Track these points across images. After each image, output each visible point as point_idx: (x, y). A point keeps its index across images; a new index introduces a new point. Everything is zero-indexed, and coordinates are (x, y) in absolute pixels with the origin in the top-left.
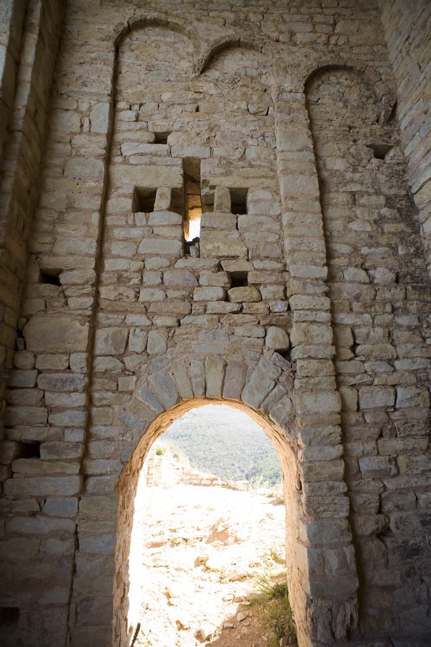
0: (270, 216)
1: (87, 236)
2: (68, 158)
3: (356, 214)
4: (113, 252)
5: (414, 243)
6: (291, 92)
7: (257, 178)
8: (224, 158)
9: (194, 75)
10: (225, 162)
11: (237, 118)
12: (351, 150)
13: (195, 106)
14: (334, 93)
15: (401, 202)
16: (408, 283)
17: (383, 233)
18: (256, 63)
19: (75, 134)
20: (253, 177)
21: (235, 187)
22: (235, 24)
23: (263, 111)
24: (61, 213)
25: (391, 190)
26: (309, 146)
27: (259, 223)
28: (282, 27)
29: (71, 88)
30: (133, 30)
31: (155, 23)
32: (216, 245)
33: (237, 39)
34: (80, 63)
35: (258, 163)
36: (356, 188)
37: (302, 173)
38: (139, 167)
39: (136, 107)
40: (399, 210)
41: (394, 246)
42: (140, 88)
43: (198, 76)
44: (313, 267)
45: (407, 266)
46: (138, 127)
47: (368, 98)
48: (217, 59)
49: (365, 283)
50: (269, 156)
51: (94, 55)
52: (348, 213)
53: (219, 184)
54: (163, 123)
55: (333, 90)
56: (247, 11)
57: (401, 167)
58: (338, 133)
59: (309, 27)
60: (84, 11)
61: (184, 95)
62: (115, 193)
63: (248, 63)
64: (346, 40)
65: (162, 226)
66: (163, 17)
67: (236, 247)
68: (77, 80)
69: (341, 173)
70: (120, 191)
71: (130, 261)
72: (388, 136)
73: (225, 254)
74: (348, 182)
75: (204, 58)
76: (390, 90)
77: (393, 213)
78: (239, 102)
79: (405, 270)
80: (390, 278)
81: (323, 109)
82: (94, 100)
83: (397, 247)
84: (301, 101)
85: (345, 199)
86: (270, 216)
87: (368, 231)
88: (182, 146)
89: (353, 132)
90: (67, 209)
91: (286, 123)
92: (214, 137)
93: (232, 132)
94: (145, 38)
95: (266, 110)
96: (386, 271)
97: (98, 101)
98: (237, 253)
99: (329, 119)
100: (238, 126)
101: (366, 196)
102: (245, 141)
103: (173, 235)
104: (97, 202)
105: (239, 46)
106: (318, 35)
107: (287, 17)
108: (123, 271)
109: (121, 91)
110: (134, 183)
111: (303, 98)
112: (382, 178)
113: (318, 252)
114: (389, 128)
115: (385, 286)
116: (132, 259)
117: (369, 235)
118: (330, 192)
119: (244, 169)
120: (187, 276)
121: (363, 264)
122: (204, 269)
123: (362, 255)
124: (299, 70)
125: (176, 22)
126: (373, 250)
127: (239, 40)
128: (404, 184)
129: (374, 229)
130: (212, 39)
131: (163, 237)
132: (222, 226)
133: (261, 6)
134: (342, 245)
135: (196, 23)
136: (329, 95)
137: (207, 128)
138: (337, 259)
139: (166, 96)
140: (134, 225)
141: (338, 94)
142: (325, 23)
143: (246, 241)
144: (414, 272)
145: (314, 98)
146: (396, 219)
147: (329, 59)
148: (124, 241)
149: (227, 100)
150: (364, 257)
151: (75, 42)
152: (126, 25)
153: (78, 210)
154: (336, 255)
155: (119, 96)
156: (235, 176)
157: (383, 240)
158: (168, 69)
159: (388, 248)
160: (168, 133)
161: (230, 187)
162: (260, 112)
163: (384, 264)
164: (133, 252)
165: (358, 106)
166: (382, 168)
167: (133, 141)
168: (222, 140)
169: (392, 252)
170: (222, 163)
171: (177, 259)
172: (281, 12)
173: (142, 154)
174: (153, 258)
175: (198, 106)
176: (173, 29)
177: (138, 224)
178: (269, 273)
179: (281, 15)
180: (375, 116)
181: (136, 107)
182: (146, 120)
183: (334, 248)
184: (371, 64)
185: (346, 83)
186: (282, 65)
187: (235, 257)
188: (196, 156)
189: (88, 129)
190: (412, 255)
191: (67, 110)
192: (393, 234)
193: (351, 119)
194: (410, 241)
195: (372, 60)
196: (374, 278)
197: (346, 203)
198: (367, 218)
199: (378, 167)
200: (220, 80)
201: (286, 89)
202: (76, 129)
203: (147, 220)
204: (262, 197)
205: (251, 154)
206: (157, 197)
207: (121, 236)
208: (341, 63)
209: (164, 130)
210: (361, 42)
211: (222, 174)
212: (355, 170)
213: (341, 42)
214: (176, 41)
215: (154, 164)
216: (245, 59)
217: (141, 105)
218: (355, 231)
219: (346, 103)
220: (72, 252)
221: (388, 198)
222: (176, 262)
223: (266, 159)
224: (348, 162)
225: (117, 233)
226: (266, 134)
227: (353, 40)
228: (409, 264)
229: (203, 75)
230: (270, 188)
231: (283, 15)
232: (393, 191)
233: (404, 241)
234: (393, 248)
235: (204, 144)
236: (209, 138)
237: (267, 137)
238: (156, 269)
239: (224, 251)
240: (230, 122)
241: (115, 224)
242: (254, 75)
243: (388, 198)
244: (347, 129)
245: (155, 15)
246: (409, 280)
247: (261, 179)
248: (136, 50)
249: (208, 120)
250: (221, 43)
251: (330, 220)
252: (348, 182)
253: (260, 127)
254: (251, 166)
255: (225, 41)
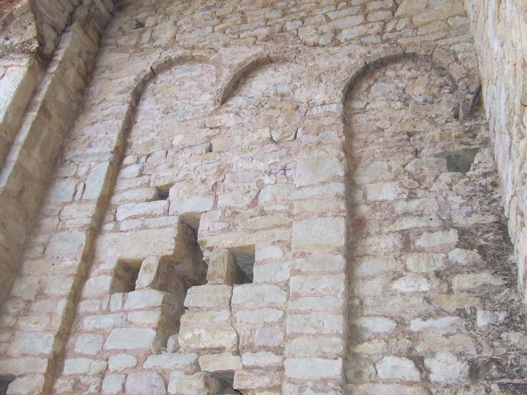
0: (277, 284)
1: (47, 330)
2: (54, 233)
3: (406, 266)
4: (76, 350)
5: (504, 305)
6: (324, 104)
7: (268, 229)
8: (230, 208)
9: (213, 108)
10: (230, 212)
11: (254, 152)
12: (408, 168)
13: (207, 145)
14: (391, 91)
15: (486, 236)
16: (492, 379)
17: (450, 292)
18: (290, 76)
19: (66, 204)
20: (262, 229)
21: (236, 246)
22: (267, 39)
23: (289, 136)
24: (29, 302)
25: (469, 218)
26: (338, 173)
27: (258, 295)
28: (325, 28)
29: (78, 152)
30: (158, 73)
31: (181, 60)
32: (197, 332)
33: (266, 56)
34: (93, 123)
35: (273, 207)
36: (407, 224)
37: (323, 215)
38: (128, 234)
39: (143, 159)
40: (482, 250)
41: (469, 312)
42: (152, 135)
43: (218, 108)
44: (320, 360)
45: (492, 346)
46: (139, 183)
47: (441, 87)
48: (244, 83)
49: (411, 384)
50: (288, 195)
51: (107, 112)
52: (392, 265)
53: (217, 244)
54: (167, 174)
55: (389, 87)
56: (285, 21)
57: (489, 179)
58: (390, 145)
59: (360, 19)
60: (111, 69)
61: (196, 135)
62: (96, 270)
63: (279, 80)
64: (408, 23)
65: (138, 310)
66: (188, 52)
67: (222, 334)
68: (84, 142)
69: (388, 204)
70: (102, 267)
71: (92, 360)
72: (471, 135)
73: (207, 345)
74: (398, 216)
75: (224, 87)
76: (469, 70)
77: (471, 256)
78: (260, 130)
79: (487, 354)
80: (458, 371)
81: (372, 117)
82: (94, 161)
83: (475, 314)
84: (336, 114)
85: (391, 244)
86: (277, 284)
87: (423, 292)
88: (181, 199)
89: (414, 140)
90: (36, 296)
91: (310, 147)
92: (223, 181)
93: (245, 170)
94: (170, 78)
95: (294, 133)
96: (453, 359)
97: (99, 162)
98: (222, 343)
99: (379, 128)
100: (255, 161)
101: (425, 234)
102: (262, 180)
103: (148, 321)
104: (68, 285)
105: (271, 62)
106: (370, 25)
107: (332, 15)
108: (80, 375)
109: (132, 144)
110: (119, 255)
111: (339, 109)
112: (456, 201)
113: (330, 335)
114: (473, 122)
115: (447, 386)
116: (94, 358)
117: (425, 298)
118: (368, 235)
119: (253, 220)
120: (154, 382)
121: (411, 349)
122: (177, 369)
123: (411, 333)
124: (337, 74)
125: (200, 54)
126: (430, 322)
127: (268, 56)
128: (494, 204)
129: (434, 286)
130: (236, 62)
131: (136, 324)
132: (210, 305)
133: (302, 11)
134: (378, 320)
135: (222, 51)
136: (384, 95)
137: (215, 170)
138: (366, 344)
139: (177, 140)
140: (108, 311)
141: (397, 91)
142: (381, 9)
143: (238, 324)
144: (505, 356)
145: (358, 105)
146: (475, 265)
147: (382, 50)
148: (92, 332)
149: (246, 129)
150: (414, 337)
151: (93, 102)
152: (149, 70)
153: (46, 297)
154: (367, 336)
155: (129, 149)
156: (239, 230)
157: (452, 305)
158: (186, 107)
159: (457, 318)
160: (171, 185)
161: (230, 247)
162: (286, 137)
163: (448, 346)
164: (98, 348)
165: (425, 101)
166: (457, 186)
167: (130, 201)
168: (230, 184)
169: (464, 323)
170: (226, 215)
171: (148, 354)
172: (326, 11)
173: (135, 217)
174: (119, 356)
175: (211, 144)
176: (200, 61)
177: (112, 309)
178: (260, 371)
179: (325, 15)
180: (450, 110)
181: (143, 159)
182: (150, 173)
183: (364, 326)
184: (442, 43)
185: (409, 74)
186: (316, 73)
187: (220, 350)
188: (195, 210)
189: (80, 196)
190: (501, 325)
191: (66, 178)
192: (468, 291)
193: (412, 122)
194: (499, 301)
195: (445, 37)
196: (429, 372)
197: (392, 250)
198: (424, 270)
199: (450, 185)
200: (243, 106)
201: (317, 102)
202: (69, 198)
203: (124, 302)
204: (269, 256)
205: (265, 197)
206: (141, 270)
207: (90, 326)
208: (399, 51)
209: (167, 182)
210: (429, 19)
211: (223, 230)
212: (412, 196)
213: (401, 26)
214: (203, 73)
215: (145, 227)
216: (277, 74)
217: (149, 156)
218: (402, 294)
219: (406, 102)
220: (26, 352)
221: (462, 232)
222: (146, 359)
223: (284, 200)
224: (401, 186)
225: (88, 323)
226: (289, 167)
227: (418, 20)
228: (496, 343)
229: (224, 105)
230: (283, 241)
231: (328, 14)
232: (474, 219)
233: (487, 301)
234: (466, 316)
235: (208, 194)
236: (216, 183)
237: (289, 169)
238: (120, 371)
239: (207, 341)
240: (244, 158)
241: (88, 310)
242: (286, 92)
243: (462, 232)
244: (406, 136)
245: (180, 52)
246: (495, 373)
247: (272, 231)
248: (158, 93)
249: (219, 160)
250: (246, 64)
251: (363, 279)
252: (398, 216)
253: (281, 158)
254: (263, 213)
255: (251, 61)
